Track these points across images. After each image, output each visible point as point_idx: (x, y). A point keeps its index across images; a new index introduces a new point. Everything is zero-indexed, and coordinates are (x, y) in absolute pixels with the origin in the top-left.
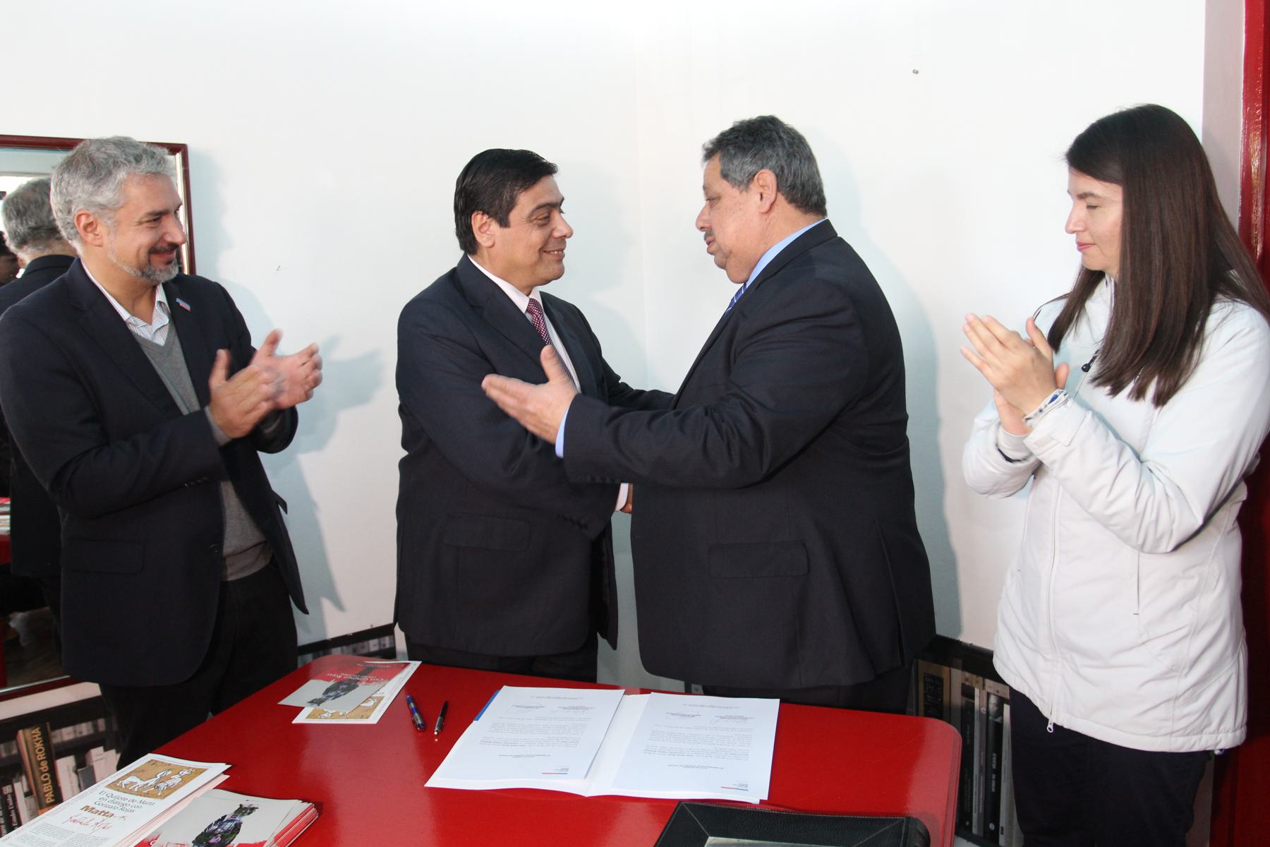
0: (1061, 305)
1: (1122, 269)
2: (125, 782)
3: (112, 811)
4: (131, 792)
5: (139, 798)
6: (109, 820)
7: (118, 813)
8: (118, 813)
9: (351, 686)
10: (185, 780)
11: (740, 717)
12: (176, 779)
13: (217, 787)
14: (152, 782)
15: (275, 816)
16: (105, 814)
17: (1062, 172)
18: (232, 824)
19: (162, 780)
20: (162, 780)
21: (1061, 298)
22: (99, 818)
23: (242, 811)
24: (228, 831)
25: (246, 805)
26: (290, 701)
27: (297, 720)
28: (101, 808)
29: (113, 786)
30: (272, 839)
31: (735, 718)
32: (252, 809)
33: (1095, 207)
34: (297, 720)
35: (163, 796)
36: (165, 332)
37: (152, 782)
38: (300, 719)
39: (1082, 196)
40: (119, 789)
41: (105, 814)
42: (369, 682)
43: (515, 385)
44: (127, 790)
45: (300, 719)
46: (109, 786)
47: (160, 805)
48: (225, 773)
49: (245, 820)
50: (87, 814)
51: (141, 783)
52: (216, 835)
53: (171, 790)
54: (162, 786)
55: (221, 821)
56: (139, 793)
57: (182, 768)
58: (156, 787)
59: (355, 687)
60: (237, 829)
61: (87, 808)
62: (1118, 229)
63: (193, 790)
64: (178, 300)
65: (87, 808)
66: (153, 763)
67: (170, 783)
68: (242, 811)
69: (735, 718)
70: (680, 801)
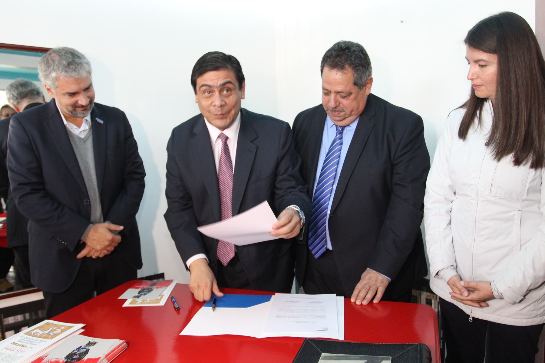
0: (463, 111)
1: (497, 95)
2: (34, 332)
3: (26, 345)
4: (36, 336)
5: (40, 339)
6: (24, 348)
7: (29, 345)
8: (29, 345)
9: (150, 290)
10: (63, 331)
11: (320, 302)
12: (59, 331)
13: (80, 334)
14: (47, 332)
15: (105, 347)
16: (22, 346)
17: (464, 48)
18: (85, 350)
19: (52, 331)
20: (52, 331)
21: (462, 107)
22: (19, 348)
23: (90, 344)
24: (82, 353)
25: (92, 341)
26: (122, 297)
27: (124, 306)
28: (20, 343)
29: (28, 333)
30: (104, 356)
31: (316, 302)
32: (95, 343)
33: (485, 66)
34: (124, 306)
35: (52, 338)
36: (86, 133)
37: (47, 332)
38: (126, 305)
39: (476, 62)
40: (30, 335)
41: (22, 346)
42: (157, 288)
43: (75, 127)
44: (34, 335)
45: (126, 305)
46: (26, 334)
47: (50, 342)
48: (83, 328)
49: (91, 348)
50: (14, 346)
51: (41, 332)
52: (76, 355)
53: (55, 335)
54: (52, 334)
55: (79, 349)
56: (40, 337)
57: (62, 326)
58: (49, 334)
59: (152, 290)
60: (87, 352)
61: (14, 343)
62: (495, 77)
63: (66, 336)
64: (97, 119)
65: (14, 343)
66: (48, 324)
67: (55, 332)
68: (90, 344)
69: (316, 302)
70: (306, 338)
